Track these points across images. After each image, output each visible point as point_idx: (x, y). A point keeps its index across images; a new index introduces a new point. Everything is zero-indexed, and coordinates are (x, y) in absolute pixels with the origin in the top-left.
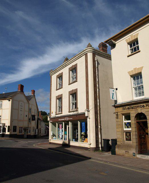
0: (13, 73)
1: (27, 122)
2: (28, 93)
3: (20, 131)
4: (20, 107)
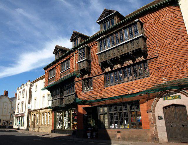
0: (11, 67)
1: (9, 117)
2: (10, 95)
3: (4, 123)
4: (4, 106)
